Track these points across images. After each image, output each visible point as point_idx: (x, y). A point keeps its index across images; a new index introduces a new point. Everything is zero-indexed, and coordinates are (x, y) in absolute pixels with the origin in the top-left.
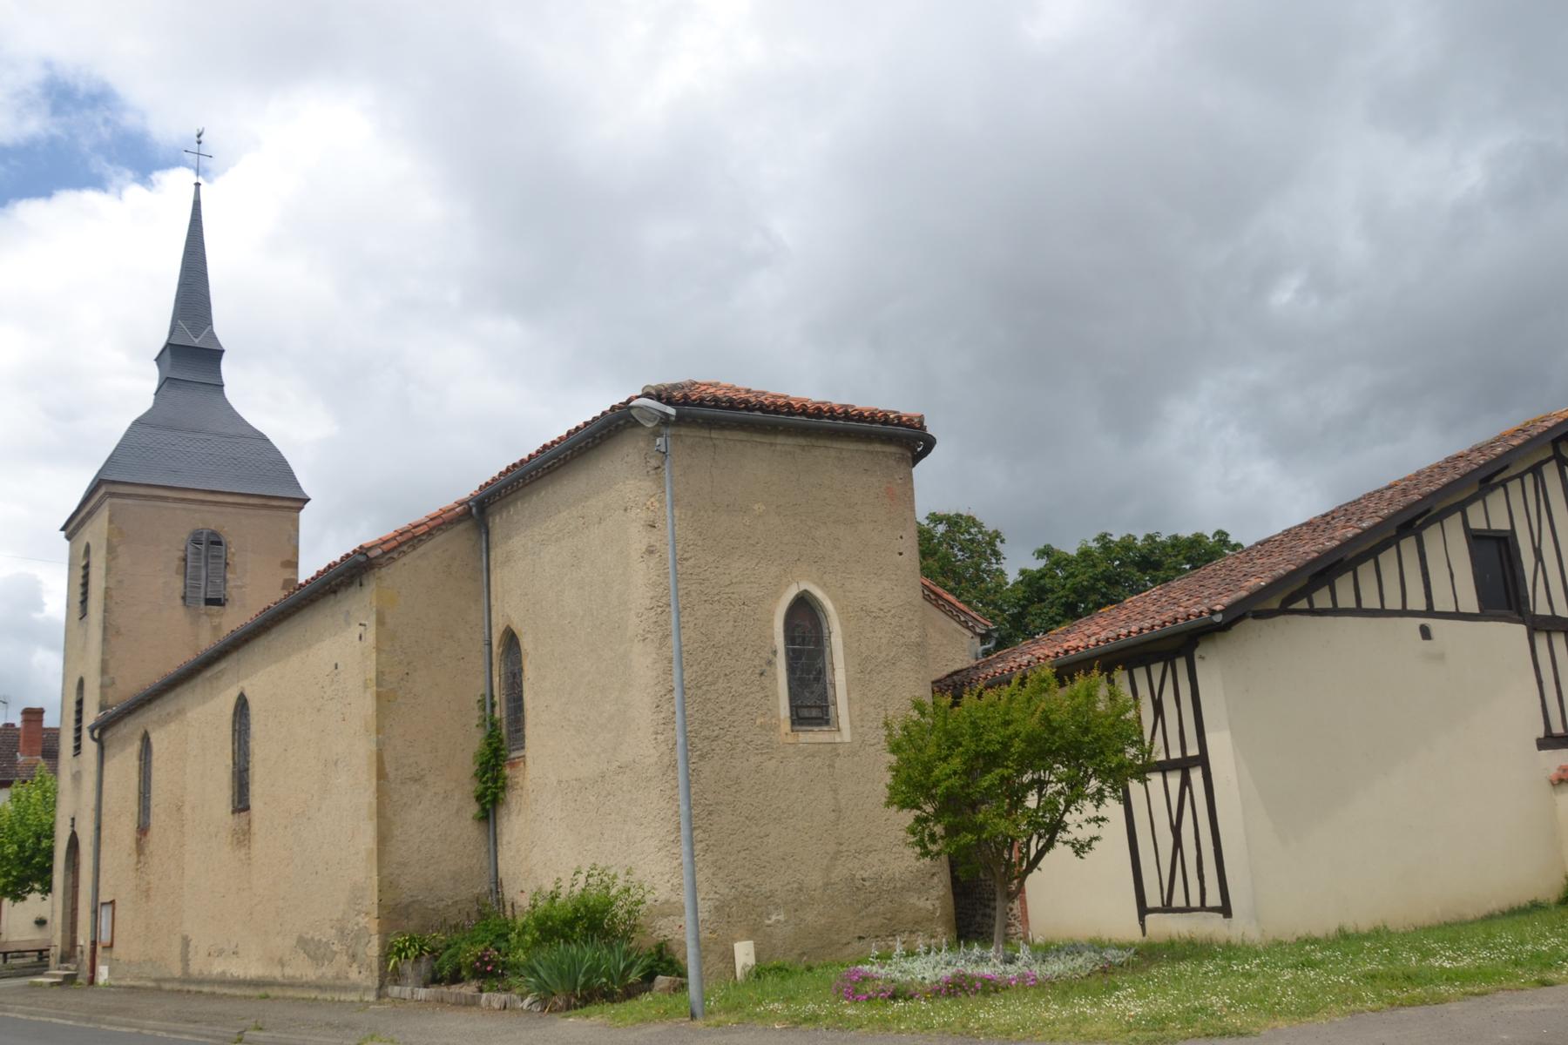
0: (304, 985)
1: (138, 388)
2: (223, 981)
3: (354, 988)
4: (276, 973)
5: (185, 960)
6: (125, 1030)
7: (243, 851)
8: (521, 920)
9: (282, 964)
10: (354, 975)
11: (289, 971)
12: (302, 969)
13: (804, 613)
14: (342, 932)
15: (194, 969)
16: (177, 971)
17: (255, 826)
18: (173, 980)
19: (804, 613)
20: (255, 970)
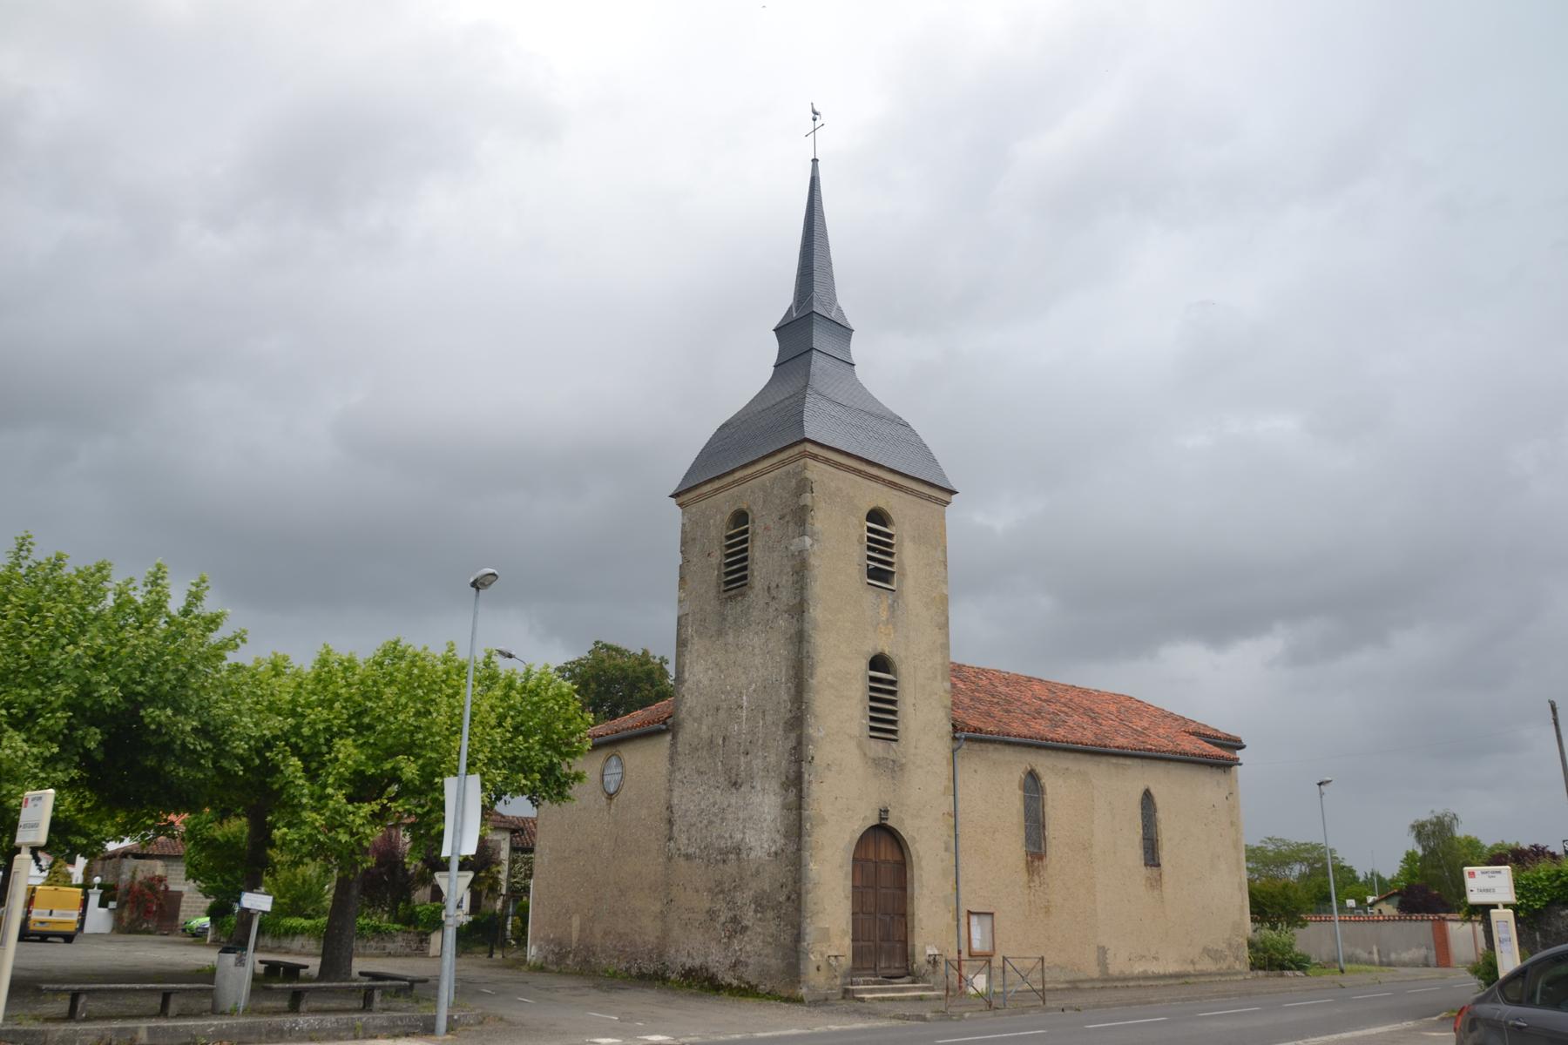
0: (1210, 974)
1: (751, 365)
2: (1146, 977)
3: (1239, 973)
4: (1190, 969)
5: (1103, 963)
6: (137, 986)
7: (1156, 893)
8: (574, 945)
9: (1193, 962)
10: (1238, 967)
11: (1198, 967)
12: (1207, 965)
13: (1147, 797)
14: (1230, 945)
15: (1114, 970)
16: (1094, 972)
17: (1165, 878)
18: (1092, 980)
19: (1147, 797)
20: (1172, 968)
